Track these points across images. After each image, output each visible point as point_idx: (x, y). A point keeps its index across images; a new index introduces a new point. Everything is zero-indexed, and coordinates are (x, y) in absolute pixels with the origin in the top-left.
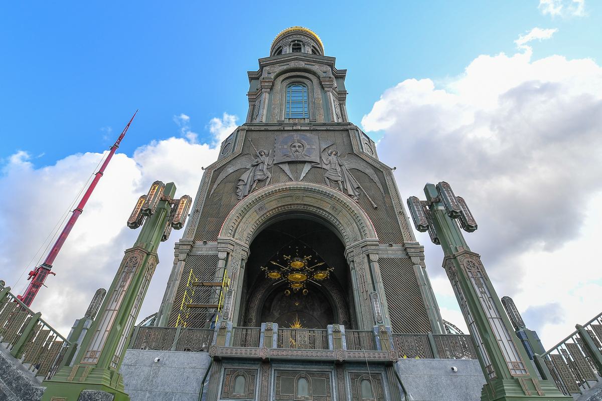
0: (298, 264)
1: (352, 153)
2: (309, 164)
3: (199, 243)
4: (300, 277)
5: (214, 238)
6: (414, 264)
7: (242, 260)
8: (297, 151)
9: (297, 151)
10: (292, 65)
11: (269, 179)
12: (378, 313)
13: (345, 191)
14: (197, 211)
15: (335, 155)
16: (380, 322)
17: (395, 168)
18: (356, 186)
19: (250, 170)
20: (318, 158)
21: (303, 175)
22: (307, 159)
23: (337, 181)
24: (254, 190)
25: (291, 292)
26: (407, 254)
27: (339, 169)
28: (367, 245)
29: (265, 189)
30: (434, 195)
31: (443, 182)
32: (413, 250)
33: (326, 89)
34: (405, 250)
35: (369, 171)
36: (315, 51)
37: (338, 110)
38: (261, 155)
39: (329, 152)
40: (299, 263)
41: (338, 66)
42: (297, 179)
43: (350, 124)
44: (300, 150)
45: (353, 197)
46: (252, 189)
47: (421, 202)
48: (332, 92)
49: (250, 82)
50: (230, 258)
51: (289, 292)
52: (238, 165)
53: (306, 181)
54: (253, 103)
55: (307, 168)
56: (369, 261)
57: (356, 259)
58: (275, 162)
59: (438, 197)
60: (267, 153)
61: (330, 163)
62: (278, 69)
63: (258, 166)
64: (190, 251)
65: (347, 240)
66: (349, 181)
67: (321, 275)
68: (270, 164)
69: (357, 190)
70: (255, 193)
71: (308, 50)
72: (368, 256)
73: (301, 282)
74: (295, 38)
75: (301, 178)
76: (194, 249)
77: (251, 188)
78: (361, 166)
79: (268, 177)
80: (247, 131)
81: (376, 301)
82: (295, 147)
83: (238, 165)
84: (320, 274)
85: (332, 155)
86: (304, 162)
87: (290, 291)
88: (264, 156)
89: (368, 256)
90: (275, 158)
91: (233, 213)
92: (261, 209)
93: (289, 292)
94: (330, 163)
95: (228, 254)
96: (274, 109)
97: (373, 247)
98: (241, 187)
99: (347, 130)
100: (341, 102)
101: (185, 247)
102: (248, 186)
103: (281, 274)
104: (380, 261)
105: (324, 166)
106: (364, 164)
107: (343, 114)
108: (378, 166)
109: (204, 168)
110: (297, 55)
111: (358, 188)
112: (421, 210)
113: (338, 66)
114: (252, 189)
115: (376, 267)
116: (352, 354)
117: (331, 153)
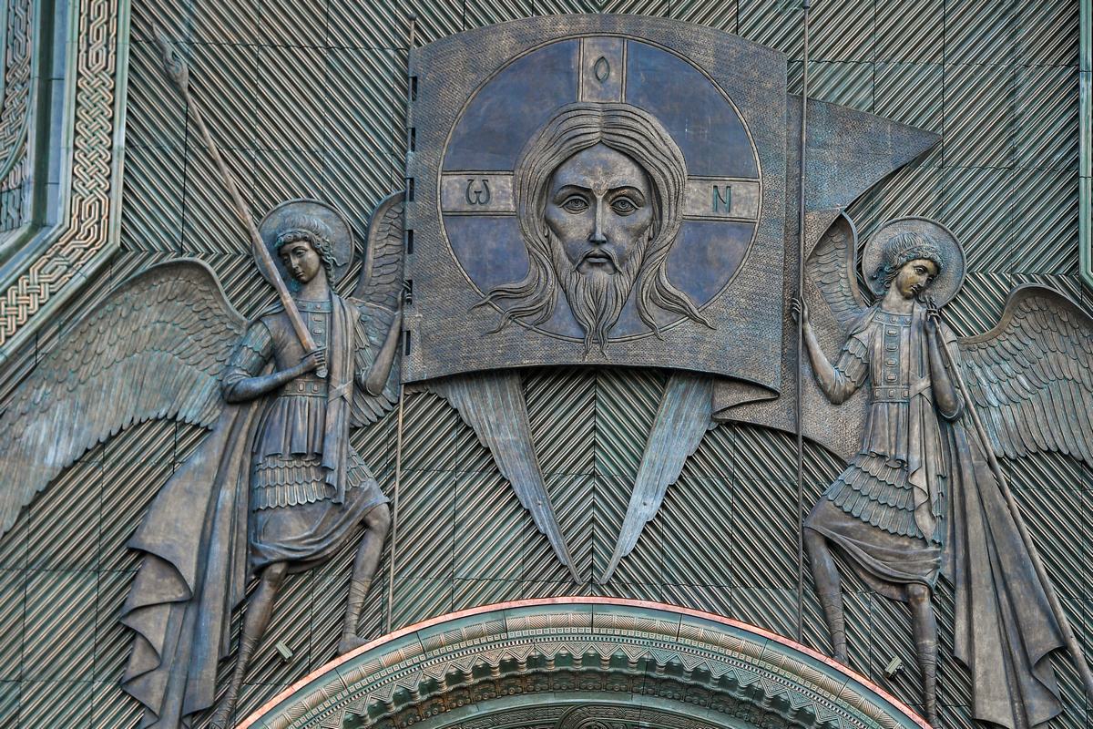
2: (694, 387)
9: (594, 254)
19: (219, 438)
20: (772, 336)
27: (924, 448)
58: (417, 366)
61: (868, 376)
63: (283, 401)
66: (1000, 580)
68: (374, 372)
82: (581, 198)
90: (413, 318)
94: (868, 376)
96: (560, 305)
98: (155, 628)
105: (820, 421)
116: (616, 158)
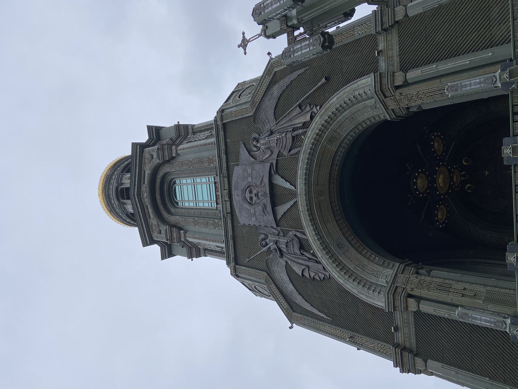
0: (421, 183)
1: (254, 117)
3: (399, 337)
4: (441, 176)
5: (390, 316)
6: (406, 15)
7: (417, 273)
8: (257, 195)
10: (147, 201)
11: (298, 234)
12: (480, 83)
13: (306, 125)
14: (351, 337)
15: (258, 141)
16: (495, 80)
17: (269, 54)
18: (298, 110)
21: (288, 185)
22: (266, 180)
23: (293, 138)
24: (314, 255)
25: (468, 184)
26: (392, 27)
28: (381, 90)
29: (310, 239)
30: (274, 26)
31: (252, 15)
32: (385, 19)
33: (174, 155)
34: (385, 30)
35: (276, 91)
36: (127, 169)
37: (202, 135)
38: (267, 244)
39: (255, 149)
40: (419, 181)
41: (144, 138)
42: (294, 195)
43: (216, 120)
44: (255, 192)
45: (313, 114)
46: (313, 258)
47: (289, 43)
48: (178, 146)
49: (175, 255)
50: (416, 292)
51: (468, 185)
52: (282, 276)
53: (296, 181)
54: (202, 252)
55: (279, 181)
56: (406, 84)
57: (404, 103)
59: (278, 19)
60: (263, 236)
62: (153, 220)
64: (411, 351)
65: (377, 119)
66: (290, 120)
67: (437, 146)
69: (303, 107)
70: (319, 254)
71: (127, 182)
72: (397, 87)
73: (450, 171)
74: (113, 196)
75: (293, 188)
76: (408, 345)
77: (312, 259)
78: (270, 104)
79: (295, 235)
80: (236, 263)
81: (462, 87)
82: (251, 198)
83: (282, 276)
84: (436, 147)
85: (258, 145)
86: (272, 186)
87: (466, 185)
88: (268, 241)
89: (397, 87)
91: (351, 287)
92: (340, 246)
93: (468, 185)
95: (410, 296)
97: (384, 81)
99: (224, 125)
100: (190, 131)
101: (405, 359)
102: (310, 264)
103: (439, 205)
104: (404, 69)
105: (275, 156)
106: (266, 99)
107: (205, 128)
108: (268, 79)
109: (290, 325)
110: (134, 192)
111: (300, 106)
112: (299, 46)
113: (144, 138)
114: (313, 258)
115: (413, 74)
117: (256, 146)
